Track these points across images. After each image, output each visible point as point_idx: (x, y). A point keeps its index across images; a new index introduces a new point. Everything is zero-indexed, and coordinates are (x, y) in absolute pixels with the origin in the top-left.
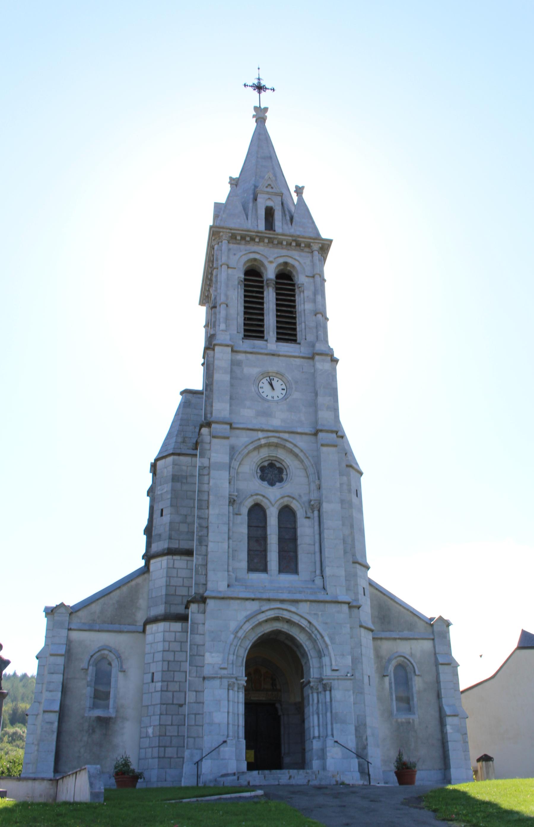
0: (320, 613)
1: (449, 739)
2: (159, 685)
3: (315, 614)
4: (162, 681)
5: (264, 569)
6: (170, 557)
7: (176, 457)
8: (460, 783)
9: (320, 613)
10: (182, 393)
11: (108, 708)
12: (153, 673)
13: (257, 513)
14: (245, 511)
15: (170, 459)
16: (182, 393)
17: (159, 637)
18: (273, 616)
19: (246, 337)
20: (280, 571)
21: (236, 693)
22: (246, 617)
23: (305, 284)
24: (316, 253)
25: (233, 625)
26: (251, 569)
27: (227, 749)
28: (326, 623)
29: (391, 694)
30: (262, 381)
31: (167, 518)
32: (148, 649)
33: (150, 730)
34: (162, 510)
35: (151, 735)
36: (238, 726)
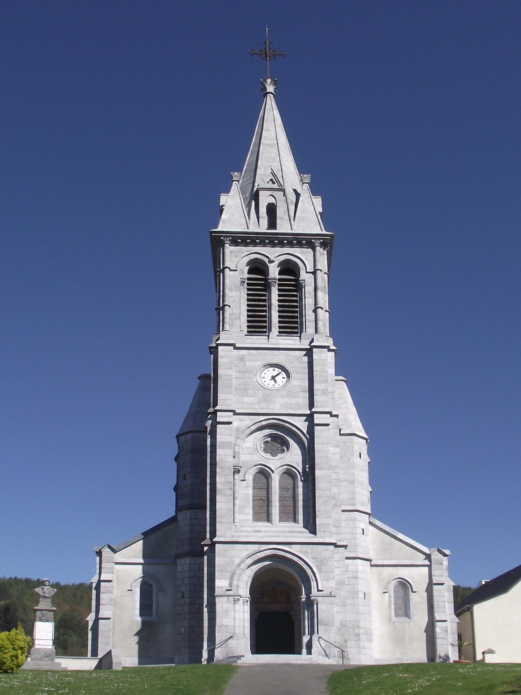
0: (310, 551)
1: (437, 637)
2: (187, 600)
3: (305, 552)
4: (190, 598)
5: (269, 519)
6: (192, 511)
7: (194, 434)
8: (88, 625)
9: (310, 551)
10: (199, 378)
11: (456, 590)
12: (183, 593)
13: (264, 473)
14: (250, 478)
15: (189, 435)
16: (199, 378)
17: (186, 567)
18: (252, 562)
19: (250, 333)
20: (281, 520)
21: (242, 606)
22: (247, 555)
23: (306, 280)
24: (318, 248)
25: (237, 561)
26: (257, 518)
27: (233, 641)
28: (315, 558)
29: (390, 605)
30: (264, 372)
31: (188, 482)
32: (178, 575)
33: (183, 630)
34: (185, 475)
35: (183, 633)
36: (244, 627)
